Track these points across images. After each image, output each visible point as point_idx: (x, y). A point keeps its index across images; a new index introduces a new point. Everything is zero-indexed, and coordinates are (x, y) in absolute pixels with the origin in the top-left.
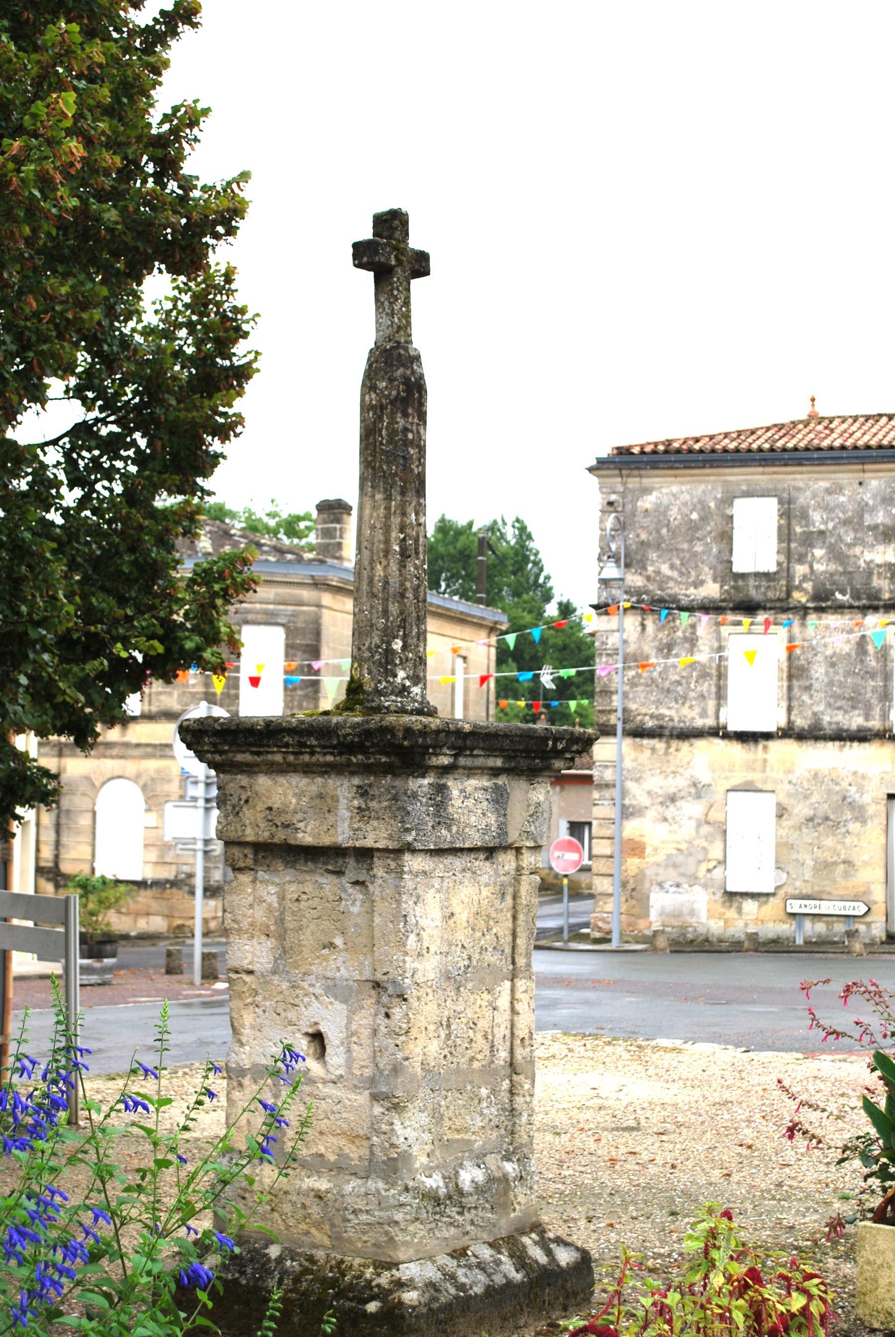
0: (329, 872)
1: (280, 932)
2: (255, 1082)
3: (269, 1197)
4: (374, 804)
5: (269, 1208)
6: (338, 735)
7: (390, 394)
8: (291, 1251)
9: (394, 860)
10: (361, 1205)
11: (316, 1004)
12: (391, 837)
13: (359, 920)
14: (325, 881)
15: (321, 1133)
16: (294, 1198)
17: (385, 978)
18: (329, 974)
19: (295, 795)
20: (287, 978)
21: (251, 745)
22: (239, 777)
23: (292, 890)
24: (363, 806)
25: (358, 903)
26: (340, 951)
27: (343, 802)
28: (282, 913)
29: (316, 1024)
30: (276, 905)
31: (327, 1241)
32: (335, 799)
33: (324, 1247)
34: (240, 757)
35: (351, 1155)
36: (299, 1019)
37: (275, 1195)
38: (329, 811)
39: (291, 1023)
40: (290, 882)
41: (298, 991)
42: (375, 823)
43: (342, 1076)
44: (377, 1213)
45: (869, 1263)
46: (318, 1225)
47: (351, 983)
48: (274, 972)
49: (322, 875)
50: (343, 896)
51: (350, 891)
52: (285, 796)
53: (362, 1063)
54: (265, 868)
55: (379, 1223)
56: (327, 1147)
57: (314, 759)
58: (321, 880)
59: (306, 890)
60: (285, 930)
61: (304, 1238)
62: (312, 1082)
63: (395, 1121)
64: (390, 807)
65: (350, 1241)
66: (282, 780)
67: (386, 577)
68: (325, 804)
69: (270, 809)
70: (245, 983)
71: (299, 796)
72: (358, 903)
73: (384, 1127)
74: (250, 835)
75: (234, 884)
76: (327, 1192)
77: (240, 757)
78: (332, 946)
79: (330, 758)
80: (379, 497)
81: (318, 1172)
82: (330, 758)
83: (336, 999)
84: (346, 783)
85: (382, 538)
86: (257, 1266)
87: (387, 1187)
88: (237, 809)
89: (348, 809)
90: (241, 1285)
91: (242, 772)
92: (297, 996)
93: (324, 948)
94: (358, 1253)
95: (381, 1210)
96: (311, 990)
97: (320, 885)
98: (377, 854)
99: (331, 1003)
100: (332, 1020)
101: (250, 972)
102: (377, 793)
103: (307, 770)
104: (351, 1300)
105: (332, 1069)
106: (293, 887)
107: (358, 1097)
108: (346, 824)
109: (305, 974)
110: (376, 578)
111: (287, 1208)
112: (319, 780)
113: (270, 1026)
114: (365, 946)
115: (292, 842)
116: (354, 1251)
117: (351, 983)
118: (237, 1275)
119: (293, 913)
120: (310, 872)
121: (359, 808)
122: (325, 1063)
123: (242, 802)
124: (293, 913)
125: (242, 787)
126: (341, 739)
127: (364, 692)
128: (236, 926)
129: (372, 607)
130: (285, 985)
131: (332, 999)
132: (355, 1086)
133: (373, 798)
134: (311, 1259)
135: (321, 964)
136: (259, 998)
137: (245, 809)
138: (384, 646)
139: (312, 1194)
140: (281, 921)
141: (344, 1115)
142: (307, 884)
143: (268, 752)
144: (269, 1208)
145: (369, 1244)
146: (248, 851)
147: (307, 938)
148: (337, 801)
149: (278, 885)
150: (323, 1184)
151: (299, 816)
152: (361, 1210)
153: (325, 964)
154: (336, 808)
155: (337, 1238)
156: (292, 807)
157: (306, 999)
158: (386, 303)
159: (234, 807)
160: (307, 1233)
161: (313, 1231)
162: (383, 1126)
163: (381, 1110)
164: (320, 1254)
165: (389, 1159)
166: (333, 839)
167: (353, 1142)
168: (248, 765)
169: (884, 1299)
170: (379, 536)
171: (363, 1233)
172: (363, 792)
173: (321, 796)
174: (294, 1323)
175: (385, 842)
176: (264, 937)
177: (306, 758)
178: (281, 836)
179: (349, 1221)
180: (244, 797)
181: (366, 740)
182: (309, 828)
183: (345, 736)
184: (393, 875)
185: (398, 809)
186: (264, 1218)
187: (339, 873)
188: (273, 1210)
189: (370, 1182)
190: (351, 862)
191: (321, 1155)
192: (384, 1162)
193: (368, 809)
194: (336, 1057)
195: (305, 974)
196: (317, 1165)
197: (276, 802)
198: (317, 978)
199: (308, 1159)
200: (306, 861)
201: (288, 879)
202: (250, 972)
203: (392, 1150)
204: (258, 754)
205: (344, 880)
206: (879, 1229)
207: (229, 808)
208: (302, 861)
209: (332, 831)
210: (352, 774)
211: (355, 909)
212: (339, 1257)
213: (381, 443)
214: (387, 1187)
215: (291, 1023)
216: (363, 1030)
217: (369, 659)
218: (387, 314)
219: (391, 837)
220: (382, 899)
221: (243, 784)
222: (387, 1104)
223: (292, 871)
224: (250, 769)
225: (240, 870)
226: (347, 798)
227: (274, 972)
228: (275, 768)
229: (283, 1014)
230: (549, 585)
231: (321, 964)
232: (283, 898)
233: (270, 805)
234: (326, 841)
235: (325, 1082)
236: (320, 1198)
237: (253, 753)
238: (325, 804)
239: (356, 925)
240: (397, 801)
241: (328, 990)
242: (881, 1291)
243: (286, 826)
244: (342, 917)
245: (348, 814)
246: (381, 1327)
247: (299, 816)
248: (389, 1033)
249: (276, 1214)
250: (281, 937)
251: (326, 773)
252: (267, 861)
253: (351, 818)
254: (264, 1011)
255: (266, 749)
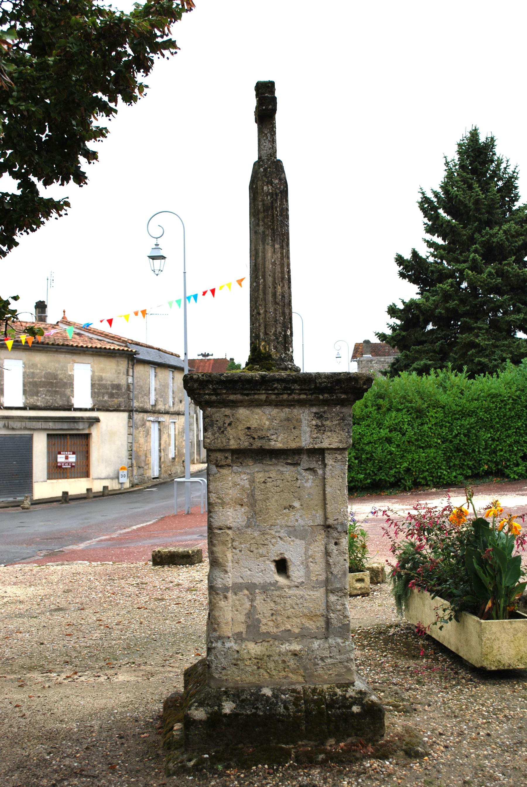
0: (288, 464)
1: (252, 502)
2: (236, 594)
3: (256, 661)
4: (328, 423)
5: (256, 667)
6: (316, 383)
7: (280, 188)
8: (279, 690)
9: (340, 454)
10: (326, 654)
11: (281, 542)
12: (341, 442)
13: (311, 491)
14: (285, 470)
15: (288, 617)
16: (276, 658)
17: (336, 522)
18: (289, 524)
19: (268, 419)
20: (258, 529)
21: (246, 389)
22: (223, 409)
23: (260, 477)
24: (320, 424)
25: (310, 481)
26: (297, 510)
27: (304, 422)
28: (252, 491)
29: (281, 554)
30: (248, 486)
31: (301, 679)
32: (299, 421)
33: (299, 683)
34: (232, 397)
35: (310, 627)
36: (268, 553)
37: (260, 661)
38: (294, 428)
39: (262, 556)
40: (258, 472)
41: (266, 536)
42: (329, 434)
43: (303, 582)
44: (338, 657)
45: (488, 639)
46: (294, 671)
47: (307, 528)
48: (248, 526)
49: (283, 466)
50: (299, 477)
51: (304, 474)
52: (261, 420)
53: (317, 573)
54: (239, 464)
55: (340, 662)
56: (293, 625)
57: (291, 397)
58: (281, 469)
59: (271, 476)
60: (256, 501)
61: (284, 680)
62: (281, 588)
63: (346, 603)
64: (339, 424)
65: (319, 676)
66: (258, 411)
67: (282, 293)
68: (292, 425)
69: (249, 428)
70: (228, 535)
71: (271, 420)
72: (310, 481)
73: (339, 607)
74: (233, 444)
75: (218, 475)
76: (301, 651)
77: (232, 397)
78: (291, 507)
79: (303, 397)
80: (277, 246)
81: (288, 641)
82: (303, 397)
83: (296, 538)
84: (307, 411)
85: (279, 270)
86: (263, 703)
87: (343, 641)
88: (222, 429)
89: (308, 426)
90: (259, 716)
91: (226, 406)
92: (267, 539)
93: (285, 509)
94: (325, 682)
95: (340, 654)
96: (277, 534)
97: (282, 473)
98: (326, 452)
99: (293, 541)
100: (294, 551)
101: (230, 528)
102: (329, 416)
103: (279, 404)
104: (339, 708)
105: (295, 579)
106: (260, 475)
107: (316, 593)
108: (308, 435)
109: (271, 525)
110: (278, 294)
111: (271, 665)
112: (287, 410)
113: (246, 559)
114: (316, 505)
115: (267, 448)
116: (321, 681)
117: (307, 528)
118: (254, 711)
119: (261, 490)
120: (276, 464)
121: (316, 426)
122: (288, 577)
123: (226, 425)
124: (261, 490)
125: (226, 416)
126: (318, 385)
127: (273, 360)
128: (220, 501)
129: (275, 310)
130: (256, 534)
131: (293, 539)
132: (313, 587)
133: (327, 419)
134: (294, 691)
135: (283, 519)
136: (235, 544)
137: (229, 429)
138: (283, 333)
139: (290, 653)
140: (252, 495)
141: (305, 605)
142: (272, 472)
143: (255, 394)
144: (256, 667)
145: (333, 675)
146: (228, 455)
147: (273, 504)
148: (301, 422)
149: (248, 474)
150: (296, 647)
151: (272, 432)
152: (327, 657)
153: (286, 518)
154: (300, 426)
155: (308, 676)
156: (266, 427)
157: (273, 541)
158: (269, 135)
159: (220, 428)
160: (286, 677)
161: (290, 675)
162: (338, 607)
163: (336, 598)
164: (299, 688)
165: (344, 625)
166: (298, 444)
167: (311, 619)
168: (232, 401)
169: (496, 655)
170: (278, 269)
171: (329, 670)
172: (319, 416)
173: (288, 419)
174: (302, 730)
175: (336, 444)
176: (239, 507)
177: (285, 397)
178: (257, 444)
179: (318, 664)
180: (228, 421)
181: (337, 385)
182: (280, 439)
183: (321, 383)
184: (340, 463)
185: (345, 425)
186: (253, 674)
187: (296, 464)
188: (258, 668)
189: (330, 640)
190: (305, 457)
191: (289, 630)
192: (340, 627)
193: (323, 425)
194: (296, 572)
195: (271, 525)
196: (287, 636)
197: (254, 424)
198: (281, 527)
199: (279, 634)
200: (271, 459)
201: (257, 470)
202: (230, 528)
203: (345, 619)
204: (247, 395)
205: (299, 468)
206: (492, 623)
207: (216, 429)
208: (268, 459)
209: (297, 440)
210: (312, 405)
211: (308, 485)
212: (312, 686)
213: (277, 215)
214: (343, 641)
215: (262, 556)
216: (317, 554)
217: (274, 340)
218: (269, 141)
219: (341, 442)
220: (332, 477)
221: (226, 414)
222: (340, 594)
223: (261, 465)
224: (234, 405)
225: (222, 467)
226: (308, 420)
227: (248, 526)
228: (255, 403)
229: (255, 551)
230: (401, 306)
231: (283, 519)
232: (254, 482)
233: (248, 426)
234: (293, 445)
235: (289, 587)
236: (296, 655)
237: (242, 394)
238: (292, 425)
239: (309, 494)
240: (344, 420)
241: (289, 534)
242: (495, 652)
243: (260, 438)
244: (298, 490)
245: (308, 429)
246: (365, 719)
247: (272, 432)
248: (340, 553)
249: (261, 670)
250: (253, 504)
251: (292, 405)
252: (240, 460)
253: (311, 431)
254: (240, 551)
255: (256, 392)
